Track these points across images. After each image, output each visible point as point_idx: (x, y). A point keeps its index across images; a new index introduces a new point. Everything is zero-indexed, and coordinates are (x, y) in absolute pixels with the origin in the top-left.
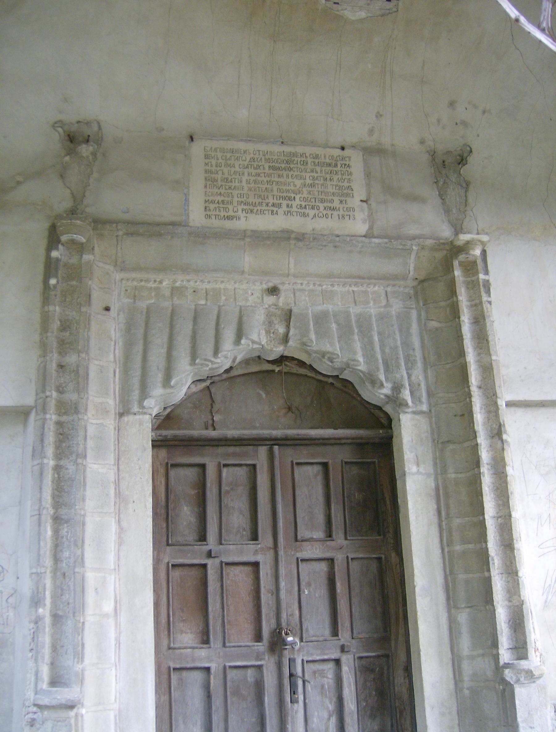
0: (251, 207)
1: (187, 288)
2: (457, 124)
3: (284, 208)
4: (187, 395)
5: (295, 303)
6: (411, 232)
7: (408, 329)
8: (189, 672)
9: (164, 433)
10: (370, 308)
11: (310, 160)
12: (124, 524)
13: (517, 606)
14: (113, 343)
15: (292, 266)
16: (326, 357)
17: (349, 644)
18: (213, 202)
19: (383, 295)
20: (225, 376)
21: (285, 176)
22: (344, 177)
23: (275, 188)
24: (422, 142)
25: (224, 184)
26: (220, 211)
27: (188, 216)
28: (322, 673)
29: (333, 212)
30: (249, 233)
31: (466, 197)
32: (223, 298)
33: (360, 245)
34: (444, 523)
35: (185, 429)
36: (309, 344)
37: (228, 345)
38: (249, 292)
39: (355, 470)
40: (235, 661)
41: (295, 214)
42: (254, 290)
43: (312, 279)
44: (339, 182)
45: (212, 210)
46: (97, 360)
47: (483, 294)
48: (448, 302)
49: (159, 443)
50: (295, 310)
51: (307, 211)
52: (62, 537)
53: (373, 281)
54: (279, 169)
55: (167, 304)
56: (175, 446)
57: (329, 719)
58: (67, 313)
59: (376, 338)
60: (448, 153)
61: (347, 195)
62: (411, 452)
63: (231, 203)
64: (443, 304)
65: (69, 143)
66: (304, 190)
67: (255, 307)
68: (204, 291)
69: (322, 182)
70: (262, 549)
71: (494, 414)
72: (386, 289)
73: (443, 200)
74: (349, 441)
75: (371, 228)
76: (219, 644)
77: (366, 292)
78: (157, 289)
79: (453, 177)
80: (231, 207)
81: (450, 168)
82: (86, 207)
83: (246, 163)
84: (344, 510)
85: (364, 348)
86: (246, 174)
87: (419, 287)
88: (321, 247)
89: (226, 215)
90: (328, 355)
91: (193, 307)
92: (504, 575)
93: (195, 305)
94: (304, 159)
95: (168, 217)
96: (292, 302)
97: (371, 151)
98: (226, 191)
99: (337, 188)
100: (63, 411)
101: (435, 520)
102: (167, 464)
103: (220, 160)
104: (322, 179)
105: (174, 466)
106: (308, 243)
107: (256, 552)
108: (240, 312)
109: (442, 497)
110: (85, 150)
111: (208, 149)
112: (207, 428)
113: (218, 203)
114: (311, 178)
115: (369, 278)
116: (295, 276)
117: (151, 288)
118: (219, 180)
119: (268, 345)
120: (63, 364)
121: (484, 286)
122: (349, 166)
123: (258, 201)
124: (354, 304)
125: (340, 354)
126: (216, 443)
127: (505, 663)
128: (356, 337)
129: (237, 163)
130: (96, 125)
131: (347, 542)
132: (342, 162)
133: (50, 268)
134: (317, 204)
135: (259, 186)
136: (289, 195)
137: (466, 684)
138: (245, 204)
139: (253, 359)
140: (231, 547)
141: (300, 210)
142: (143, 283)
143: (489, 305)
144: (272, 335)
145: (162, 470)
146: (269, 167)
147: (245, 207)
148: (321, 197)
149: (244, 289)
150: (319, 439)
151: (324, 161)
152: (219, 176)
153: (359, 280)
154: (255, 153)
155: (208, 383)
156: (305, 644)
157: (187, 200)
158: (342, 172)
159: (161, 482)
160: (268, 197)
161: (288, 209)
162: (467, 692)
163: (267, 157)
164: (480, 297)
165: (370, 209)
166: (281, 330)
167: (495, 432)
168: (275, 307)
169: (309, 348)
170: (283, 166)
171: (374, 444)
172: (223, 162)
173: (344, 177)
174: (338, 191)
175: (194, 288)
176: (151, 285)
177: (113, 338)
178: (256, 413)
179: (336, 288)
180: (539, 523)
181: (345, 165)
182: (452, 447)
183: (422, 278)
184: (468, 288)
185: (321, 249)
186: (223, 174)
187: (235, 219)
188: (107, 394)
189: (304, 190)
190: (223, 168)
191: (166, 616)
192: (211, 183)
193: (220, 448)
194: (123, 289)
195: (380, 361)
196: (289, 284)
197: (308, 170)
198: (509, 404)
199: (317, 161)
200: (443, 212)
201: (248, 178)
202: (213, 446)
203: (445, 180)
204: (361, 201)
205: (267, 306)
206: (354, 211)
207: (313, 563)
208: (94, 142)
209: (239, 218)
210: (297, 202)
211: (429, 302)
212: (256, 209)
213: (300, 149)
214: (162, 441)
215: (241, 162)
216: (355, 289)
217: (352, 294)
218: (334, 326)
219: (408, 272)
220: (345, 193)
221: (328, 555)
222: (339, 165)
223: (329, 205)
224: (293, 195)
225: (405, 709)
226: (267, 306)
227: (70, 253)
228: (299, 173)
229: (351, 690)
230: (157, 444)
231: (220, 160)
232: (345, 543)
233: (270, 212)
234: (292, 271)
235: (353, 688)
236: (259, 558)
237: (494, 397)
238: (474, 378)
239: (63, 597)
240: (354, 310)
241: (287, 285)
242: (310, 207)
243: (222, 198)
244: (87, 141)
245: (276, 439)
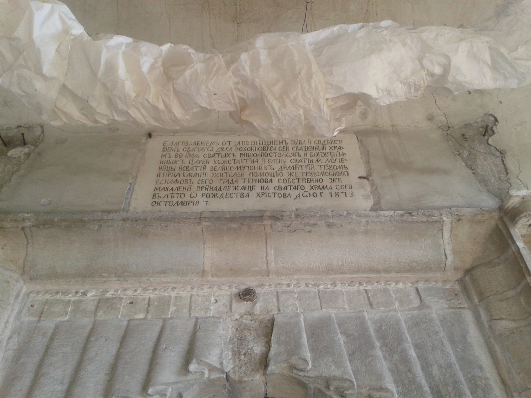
0: (215, 192)
1: (121, 299)
3: (258, 189)
5: (279, 310)
7: (464, 337)
10: (395, 310)
15: (271, 258)
16: (332, 388)
19: (413, 295)
22: (334, 158)
26: (172, 197)
29: (322, 191)
32: (173, 308)
33: (364, 220)
36: (302, 367)
43: (303, 277)
44: (329, 162)
48: (519, 289)
50: (279, 319)
51: (287, 192)
53: (393, 275)
55: (87, 321)
59: (412, 353)
60: (468, 125)
63: (189, 189)
64: (511, 293)
67: (219, 318)
68: (147, 302)
69: (307, 163)
72: (416, 285)
73: (473, 170)
77: (386, 291)
78: (77, 303)
79: (481, 148)
80: (188, 193)
83: (212, 153)
85: (395, 371)
88: (309, 228)
89: (180, 200)
90: (335, 384)
91: (125, 323)
93: (129, 321)
96: (275, 308)
98: (184, 179)
99: (327, 168)
103: (181, 152)
106: (288, 223)
108: (196, 325)
116: (278, 274)
117: (69, 302)
119: (234, 373)
122: (340, 148)
124: (369, 307)
125: (354, 381)
128: (379, 353)
134: (301, 184)
136: (264, 178)
142: (58, 296)
144: (242, 357)
147: (206, 192)
149: (204, 296)
151: (309, 145)
153: (372, 275)
154: (224, 143)
158: (333, 154)
163: (239, 146)
165: (373, 184)
166: (258, 349)
168: (250, 317)
169: (301, 374)
172: (184, 154)
173: (334, 158)
174: (328, 171)
175: (131, 298)
176: (71, 297)
179: (339, 287)
181: (335, 147)
183: (468, 265)
185: (310, 232)
187: (191, 205)
189: (285, 172)
190: (183, 158)
192: (166, 171)
194: (29, 304)
195: (427, 389)
197: (290, 154)
201: (214, 165)
203: (470, 152)
204: (360, 178)
205: (237, 317)
208: (31, 145)
210: (276, 183)
211: (488, 295)
212: (220, 193)
215: (207, 152)
216: (369, 288)
217: (365, 294)
218: (341, 339)
224: (269, 178)
226: (237, 317)
233: (239, 195)
240: (370, 316)
241: (267, 287)
242: (292, 188)
243: (178, 185)
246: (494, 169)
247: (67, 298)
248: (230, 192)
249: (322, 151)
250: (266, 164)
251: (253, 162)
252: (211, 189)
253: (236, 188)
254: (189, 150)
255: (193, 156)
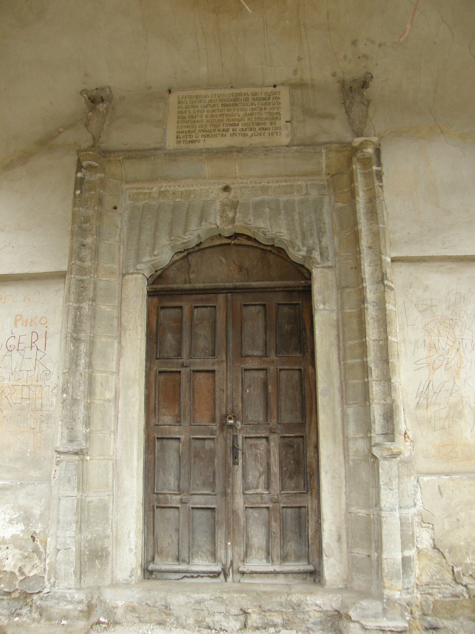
0: (208, 133)
1: (168, 191)
2: (359, 58)
3: (231, 131)
4: (172, 262)
6: (322, 140)
7: (321, 209)
8: (167, 440)
9: (155, 286)
11: (250, 97)
12: (123, 344)
13: (390, 404)
14: (118, 230)
15: (237, 171)
17: (275, 427)
18: (182, 132)
20: (197, 248)
21: (232, 110)
22: (274, 106)
23: (225, 118)
24: (334, 75)
25: (190, 119)
26: (187, 138)
27: (165, 143)
28: (256, 446)
29: (265, 131)
30: (204, 151)
31: (367, 111)
34: (341, 344)
35: (170, 284)
37: (193, 227)
38: (210, 191)
39: (286, 310)
40: (197, 435)
41: (238, 135)
42: (213, 189)
45: (181, 137)
46: (107, 240)
47: (375, 180)
49: (152, 293)
52: (81, 351)
54: (228, 105)
56: (164, 295)
57: (260, 477)
58: (88, 212)
60: (354, 81)
61: (276, 118)
62: (319, 295)
64: (346, 190)
65: (91, 103)
66: (246, 118)
67: (214, 200)
68: (180, 193)
69: (258, 111)
70: (218, 362)
71: (379, 266)
73: (348, 115)
74: (281, 289)
75: (292, 140)
76: (187, 424)
77: (292, 186)
80: (194, 134)
81: (355, 90)
82: (101, 143)
83: (205, 104)
84: (276, 337)
86: (206, 111)
87: (331, 179)
88: (256, 156)
89: (191, 140)
90: (262, 230)
92: (382, 382)
94: (247, 97)
95: (153, 145)
97: (297, 86)
100: (84, 273)
101: (335, 342)
102: (158, 307)
104: (258, 109)
105: (162, 308)
107: (214, 364)
109: (341, 326)
110: (101, 107)
111: (181, 97)
112: (185, 283)
113: (186, 132)
114: (251, 109)
115: (294, 176)
117: (146, 193)
118: (187, 117)
119: (221, 225)
120: (85, 244)
121: (377, 175)
122: (279, 98)
123: (212, 128)
126: (189, 292)
127: (375, 443)
129: (199, 105)
130: (108, 90)
131: (277, 358)
132: (273, 96)
133: (79, 183)
134: (254, 127)
135: (214, 118)
136: (234, 122)
137: (351, 458)
138: (204, 132)
139: (216, 236)
140: (197, 360)
141: (241, 132)
142: (140, 191)
143: (380, 188)
144: (224, 219)
145: (154, 311)
146: (222, 105)
147: (204, 134)
148: (257, 122)
150: (259, 288)
152: (187, 115)
153: (287, 178)
155: (185, 253)
156: (245, 426)
157: (165, 133)
159: (154, 319)
160: (219, 125)
161: (233, 132)
162: (351, 463)
163: (220, 98)
164: (374, 182)
167: (380, 279)
169: (248, 226)
170: (231, 103)
171: (299, 291)
172: (190, 105)
173: (274, 106)
174: (269, 117)
177: (120, 227)
178: (218, 271)
180: (416, 346)
181: (276, 98)
182: (348, 290)
183: (333, 173)
184: (365, 177)
186: (190, 112)
188: (113, 261)
189: (246, 118)
191: (154, 404)
193: (193, 295)
196: (238, 183)
197: (249, 104)
198: (394, 260)
199: (255, 97)
200: (348, 124)
202: (188, 294)
203: (351, 101)
206: (280, 129)
207: (254, 372)
208: (107, 101)
209: (200, 141)
210: (240, 126)
212: (211, 134)
213: (244, 90)
214: (154, 292)
215: (202, 104)
219: (321, 169)
220: (275, 117)
221: (263, 366)
222: (271, 98)
223: (263, 126)
224: (237, 123)
225: (313, 474)
227: (91, 174)
228: (242, 107)
229: (275, 459)
230: (151, 294)
231: (189, 104)
232: (276, 358)
233: (221, 135)
234: (238, 175)
235: (277, 457)
236: (216, 368)
237: (380, 254)
238: (365, 242)
239: (80, 388)
240: (284, 198)
243: (189, 129)
244: (103, 101)
245: (229, 289)
246: (360, 114)
247: (144, 191)
248: (216, 133)
249: (268, 101)
250: (236, 112)
251: (228, 110)
252: (206, 131)
253: (219, 131)
254: (192, 103)
255: (195, 107)
